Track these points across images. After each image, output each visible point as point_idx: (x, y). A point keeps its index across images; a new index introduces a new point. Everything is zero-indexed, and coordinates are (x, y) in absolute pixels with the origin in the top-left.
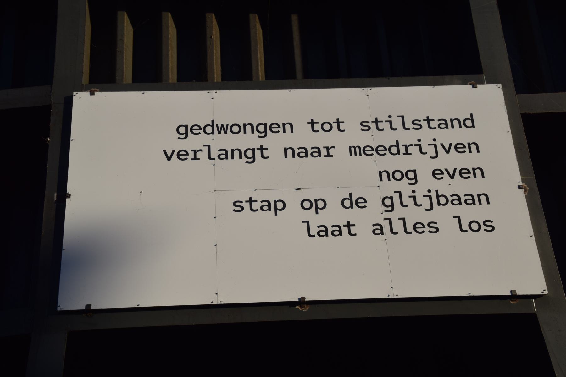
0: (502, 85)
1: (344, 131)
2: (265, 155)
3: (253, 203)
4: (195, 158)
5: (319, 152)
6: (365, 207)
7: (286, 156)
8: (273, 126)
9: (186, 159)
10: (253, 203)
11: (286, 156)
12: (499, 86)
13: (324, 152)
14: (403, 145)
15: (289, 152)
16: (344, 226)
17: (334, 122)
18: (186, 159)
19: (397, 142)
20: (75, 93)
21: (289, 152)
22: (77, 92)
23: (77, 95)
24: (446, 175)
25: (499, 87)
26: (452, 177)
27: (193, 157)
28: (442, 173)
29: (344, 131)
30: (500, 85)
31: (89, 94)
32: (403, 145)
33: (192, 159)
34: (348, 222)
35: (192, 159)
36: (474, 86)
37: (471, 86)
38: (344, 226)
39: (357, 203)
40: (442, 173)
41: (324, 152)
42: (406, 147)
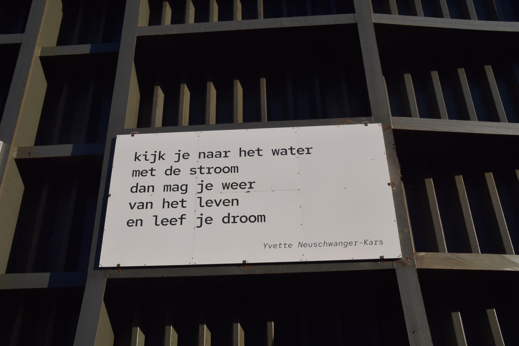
0: (382, 124)
1: (262, 155)
2: (260, 154)
3: (293, 150)
4: (308, 153)
5: (220, 155)
6: (253, 155)
7: (240, 156)
8: (250, 152)
9: (303, 153)
10: (293, 150)
11: (240, 156)
12: (380, 125)
13: (223, 154)
14: (232, 217)
15: (202, 155)
16: (289, 149)
17: (256, 150)
18: (303, 153)
19: (229, 214)
20: (117, 136)
21: (202, 155)
22: (118, 135)
23: (118, 137)
24: (214, 204)
25: (380, 125)
26: (218, 205)
27: (307, 153)
28: (212, 203)
29: (262, 155)
30: (380, 124)
31: (131, 136)
32: (232, 217)
33: (306, 154)
34: (291, 147)
35: (306, 154)
36: (366, 125)
37: (364, 125)
38: (289, 149)
39: (174, 172)
40: (212, 203)
41: (223, 154)
42: (234, 217)
